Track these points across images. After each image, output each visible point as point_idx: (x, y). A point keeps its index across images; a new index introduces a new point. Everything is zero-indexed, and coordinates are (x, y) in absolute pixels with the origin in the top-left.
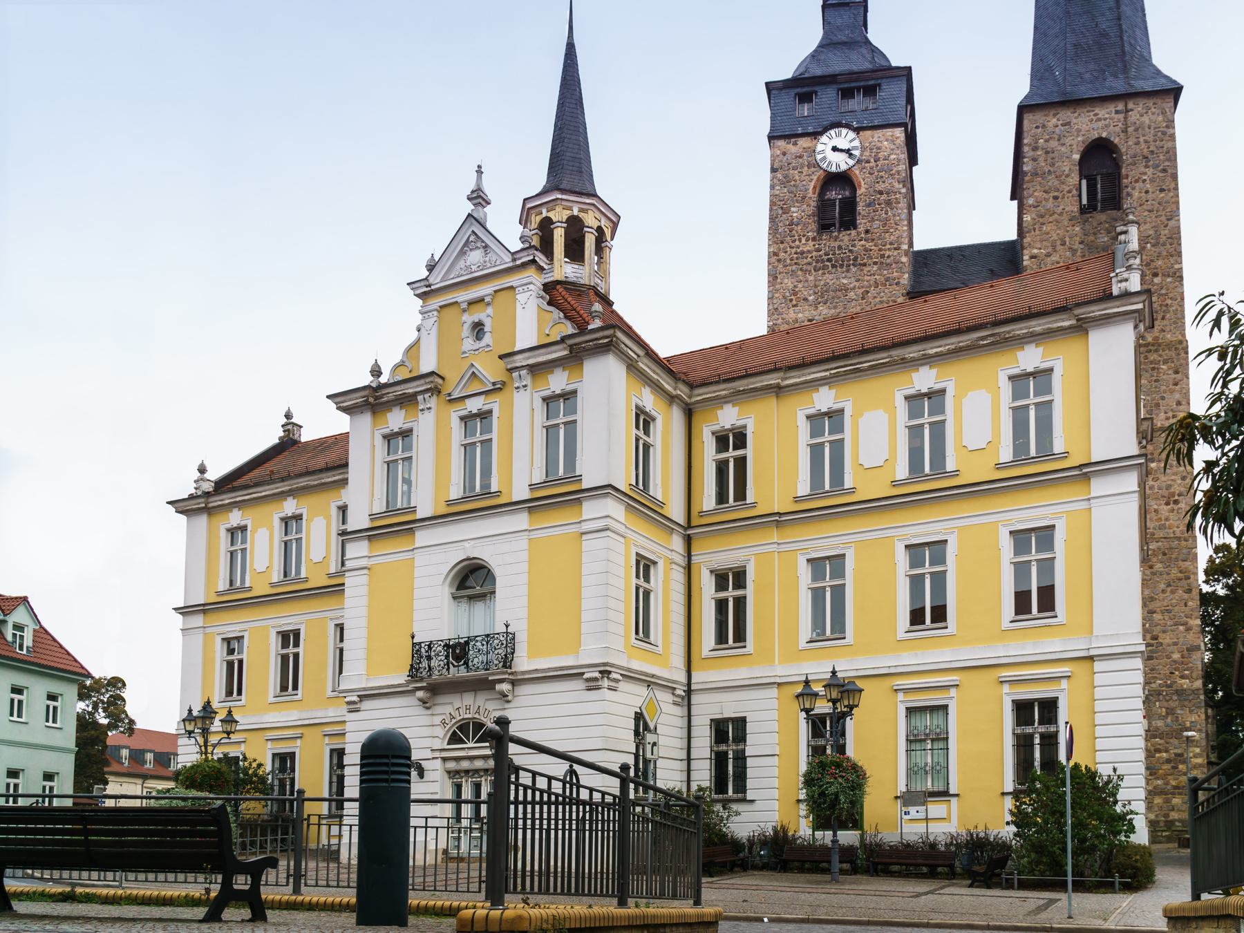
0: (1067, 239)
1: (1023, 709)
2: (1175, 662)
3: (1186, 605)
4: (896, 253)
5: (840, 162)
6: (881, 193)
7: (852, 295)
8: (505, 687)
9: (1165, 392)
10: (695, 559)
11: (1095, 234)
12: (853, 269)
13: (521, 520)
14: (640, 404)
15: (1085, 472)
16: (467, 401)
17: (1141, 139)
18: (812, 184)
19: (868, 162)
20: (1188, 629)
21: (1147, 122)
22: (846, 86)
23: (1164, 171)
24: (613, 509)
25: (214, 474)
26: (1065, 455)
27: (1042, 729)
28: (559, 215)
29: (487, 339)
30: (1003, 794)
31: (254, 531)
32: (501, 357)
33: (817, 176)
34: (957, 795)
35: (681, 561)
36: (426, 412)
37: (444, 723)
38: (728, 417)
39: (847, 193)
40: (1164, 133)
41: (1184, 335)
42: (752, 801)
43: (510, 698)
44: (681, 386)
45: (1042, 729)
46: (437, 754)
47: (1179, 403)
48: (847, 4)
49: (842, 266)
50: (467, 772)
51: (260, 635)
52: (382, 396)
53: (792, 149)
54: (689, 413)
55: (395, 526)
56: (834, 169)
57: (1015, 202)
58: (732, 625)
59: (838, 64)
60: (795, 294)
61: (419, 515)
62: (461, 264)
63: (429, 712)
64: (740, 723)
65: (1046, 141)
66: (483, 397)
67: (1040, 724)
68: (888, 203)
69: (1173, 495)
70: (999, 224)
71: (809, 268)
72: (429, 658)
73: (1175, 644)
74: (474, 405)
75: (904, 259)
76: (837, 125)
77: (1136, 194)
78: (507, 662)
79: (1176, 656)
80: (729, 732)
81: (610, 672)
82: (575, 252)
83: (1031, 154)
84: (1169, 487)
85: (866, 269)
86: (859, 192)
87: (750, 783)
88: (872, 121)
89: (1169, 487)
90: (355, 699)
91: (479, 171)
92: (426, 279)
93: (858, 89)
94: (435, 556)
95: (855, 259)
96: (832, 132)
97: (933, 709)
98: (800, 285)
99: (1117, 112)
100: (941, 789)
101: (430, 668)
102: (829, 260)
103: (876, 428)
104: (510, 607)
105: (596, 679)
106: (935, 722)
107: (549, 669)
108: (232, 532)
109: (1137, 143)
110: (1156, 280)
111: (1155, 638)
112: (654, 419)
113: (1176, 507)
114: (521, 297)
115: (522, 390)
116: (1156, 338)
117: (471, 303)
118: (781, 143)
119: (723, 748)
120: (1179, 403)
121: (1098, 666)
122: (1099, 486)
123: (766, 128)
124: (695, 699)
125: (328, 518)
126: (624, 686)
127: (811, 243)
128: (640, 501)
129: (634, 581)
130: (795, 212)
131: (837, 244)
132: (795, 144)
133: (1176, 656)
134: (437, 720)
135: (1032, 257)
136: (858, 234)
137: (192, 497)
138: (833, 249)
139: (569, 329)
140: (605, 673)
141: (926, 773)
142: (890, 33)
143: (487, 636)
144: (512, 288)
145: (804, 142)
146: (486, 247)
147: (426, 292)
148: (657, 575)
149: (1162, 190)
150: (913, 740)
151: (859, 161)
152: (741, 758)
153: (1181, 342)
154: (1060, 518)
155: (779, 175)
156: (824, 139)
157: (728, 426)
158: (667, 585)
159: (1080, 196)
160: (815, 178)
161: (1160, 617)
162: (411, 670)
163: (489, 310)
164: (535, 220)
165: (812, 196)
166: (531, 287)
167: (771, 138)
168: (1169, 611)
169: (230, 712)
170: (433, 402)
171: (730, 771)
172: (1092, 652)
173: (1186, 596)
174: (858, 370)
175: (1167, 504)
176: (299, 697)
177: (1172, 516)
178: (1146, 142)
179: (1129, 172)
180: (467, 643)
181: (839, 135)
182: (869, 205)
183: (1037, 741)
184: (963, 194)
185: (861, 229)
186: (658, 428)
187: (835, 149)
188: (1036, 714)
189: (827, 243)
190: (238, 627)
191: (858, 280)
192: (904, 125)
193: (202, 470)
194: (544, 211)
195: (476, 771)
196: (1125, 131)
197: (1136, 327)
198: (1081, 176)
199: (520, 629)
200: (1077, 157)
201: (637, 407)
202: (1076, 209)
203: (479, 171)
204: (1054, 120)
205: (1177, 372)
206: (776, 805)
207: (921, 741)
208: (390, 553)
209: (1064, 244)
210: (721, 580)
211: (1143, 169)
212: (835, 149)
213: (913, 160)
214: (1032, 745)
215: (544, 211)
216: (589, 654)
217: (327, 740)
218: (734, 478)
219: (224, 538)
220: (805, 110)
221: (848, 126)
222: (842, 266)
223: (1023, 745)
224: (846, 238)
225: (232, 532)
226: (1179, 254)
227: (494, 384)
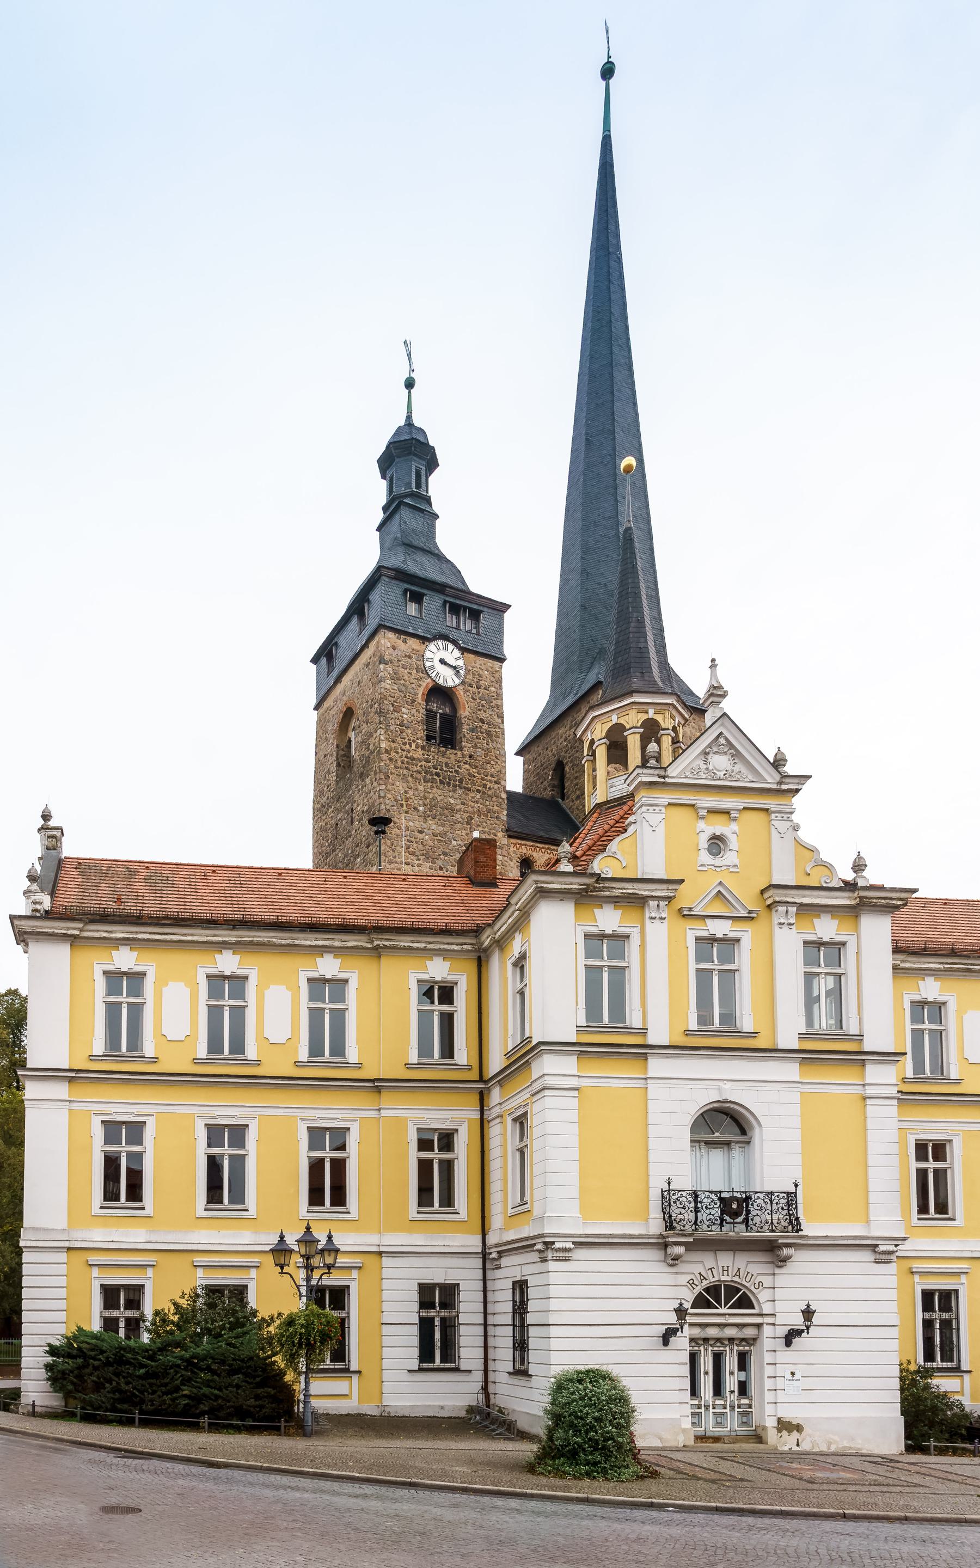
4: (496, 786)
5: (448, 678)
6: (482, 721)
12: (460, 791)
16: (708, 921)
22: (475, 607)
29: (729, 858)
31: (160, 984)
33: (426, 684)
36: (657, 922)
37: (691, 1283)
39: (448, 710)
49: (449, 784)
50: (731, 1340)
52: (601, 890)
56: (441, 682)
66: (730, 922)
68: (489, 734)
71: (419, 776)
74: (720, 928)
76: (445, 637)
81: (877, 1246)
88: (476, 646)
91: (713, 665)
94: (680, 1091)
95: (461, 781)
96: (440, 642)
98: (411, 792)
105: (569, 1250)
107: (842, 1238)
108: (113, 978)
115: (785, 928)
117: (711, 811)
125: (296, 990)
127: (420, 751)
131: (444, 760)
132: (405, 642)
134: (684, 1279)
136: (464, 756)
138: (440, 764)
145: (413, 643)
151: (463, 683)
156: (432, 646)
160: (424, 684)
163: (734, 826)
169: (308, 1228)
174: (969, 970)
176: (149, 1211)
180: (748, 1198)
181: (446, 649)
191: (463, 804)
194: (651, 712)
212: (442, 661)
215: (651, 712)
220: (412, 609)
221: (454, 642)
224: (453, 757)
225: (113, 978)
227: (750, 912)
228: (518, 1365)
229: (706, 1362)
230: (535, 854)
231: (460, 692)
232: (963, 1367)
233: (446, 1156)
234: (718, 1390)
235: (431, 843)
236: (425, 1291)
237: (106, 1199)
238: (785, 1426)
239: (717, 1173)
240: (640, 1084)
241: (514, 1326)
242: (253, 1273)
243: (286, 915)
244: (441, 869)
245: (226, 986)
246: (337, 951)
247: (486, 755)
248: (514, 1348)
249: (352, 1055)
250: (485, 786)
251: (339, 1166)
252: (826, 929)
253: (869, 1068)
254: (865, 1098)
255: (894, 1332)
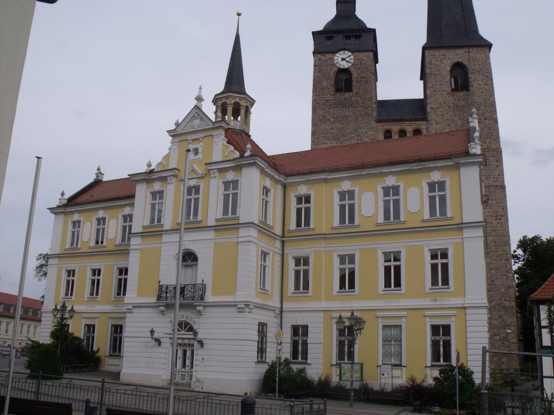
0: (446, 102)
1: (435, 329)
2: (502, 293)
3: (506, 266)
5: (345, 65)
6: (363, 78)
7: (350, 119)
8: (200, 308)
9: (493, 170)
10: (286, 251)
11: (458, 100)
12: (351, 109)
13: (211, 235)
14: (265, 185)
15: (460, 227)
17: (476, 63)
18: (332, 73)
19: (357, 65)
20: (508, 278)
21: (478, 57)
23: (487, 77)
24: (253, 233)
25: (68, 195)
26: (451, 218)
27: (444, 338)
28: (231, 101)
29: (200, 156)
30: (426, 367)
31: (109, 220)
32: (206, 164)
34: (405, 366)
35: (280, 252)
36: (170, 184)
38: (303, 190)
40: (486, 62)
41: (500, 146)
42: (310, 364)
43: (202, 313)
44: (282, 176)
45: (444, 338)
46: (167, 336)
47: (499, 175)
48: (347, 2)
51: (84, 269)
53: (323, 58)
54: (285, 186)
55: (154, 231)
56: (342, 67)
57: (422, 81)
58: (303, 283)
59: (343, 26)
60: (324, 117)
61: (165, 228)
62: (190, 124)
63: (165, 316)
64: (305, 328)
65: (436, 61)
67: (443, 335)
68: (367, 82)
69: (498, 216)
70: (414, 90)
72: (166, 293)
73: (502, 285)
74: (192, 183)
75: (374, 105)
77: (475, 85)
78: (202, 298)
79: (503, 290)
80: (300, 332)
81: (249, 305)
82: (236, 113)
83: (429, 66)
84: (496, 212)
85: (357, 109)
86: (353, 77)
87: (309, 356)
89: (496, 212)
90: (131, 307)
91: (200, 88)
92: (174, 130)
93: (353, 36)
94: (169, 250)
95: (352, 104)
96: (341, 52)
97: (395, 326)
98: (327, 114)
99: (465, 52)
100: (398, 363)
101: (167, 297)
102: (340, 104)
103: (369, 203)
104: (204, 272)
105: (243, 308)
106: (396, 333)
108: (74, 223)
109: (475, 65)
110: (486, 122)
111: (492, 281)
112: (270, 190)
113: (500, 221)
114: (216, 140)
116: (487, 146)
117: (193, 140)
118: (319, 55)
119: (297, 338)
120: (499, 175)
121: (468, 311)
122: (467, 233)
123: (312, 48)
124: (284, 315)
125: (117, 220)
126: (255, 311)
127: (332, 97)
128: (264, 229)
129: (260, 263)
130: (325, 84)
131: (343, 97)
132: (325, 56)
133: (503, 290)
135: (431, 108)
137: (59, 207)
139: (237, 154)
140: (247, 306)
141: (391, 355)
142: (365, 11)
143: (194, 285)
144: (212, 135)
145: (329, 56)
146: (202, 118)
147: (173, 134)
148: (269, 259)
149: (486, 85)
150: (386, 340)
152: (305, 344)
153: (498, 149)
154: (450, 245)
155: (317, 68)
156: (338, 55)
157: (302, 194)
158: (273, 262)
159: (451, 84)
161: (495, 272)
162: (158, 297)
163: (201, 144)
164: (220, 103)
165: (332, 77)
166: (221, 136)
167: (314, 53)
168: (499, 269)
169: (64, 303)
170: (174, 180)
171: (299, 349)
172: (465, 305)
173: (506, 262)
175: (496, 220)
176: (73, 300)
177: (498, 225)
178: (478, 64)
179: (472, 76)
181: (344, 54)
182: (358, 82)
183: (441, 343)
184: (399, 77)
185: (355, 92)
186: (271, 194)
187: (343, 59)
188: (441, 331)
189: (340, 96)
190: (73, 266)
192: (373, 51)
193: (63, 194)
195: (185, 344)
196: (469, 60)
197: (479, 167)
198: (451, 76)
199: (209, 283)
200: (449, 69)
201: (264, 186)
202: (449, 89)
203: (200, 88)
204: (438, 54)
205: (497, 161)
206: (321, 367)
207: (389, 340)
208: (151, 244)
209: (445, 103)
210: (298, 261)
211: (477, 75)
213: (376, 61)
214: (439, 345)
216: (240, 296)
217: (110, 320)
218: (304, 218)
219: (70, 225)
221: (348, 50)
222: (346, 107)
223: (435, 345)
224: (348, 95)
225: (74, 223)
226: (496, 112)
228: (259, 359)
229: (180, 354)
230: (392, 128)
231: (352, 70)
232: (403, 365)
233: (444, 261)
234: (184, 366)
235: (336, 133)
236: (435, 329)
237: (385, 287)
238: (198, 380)
239: (187, 277)
240: (159, 245)
241: (258, 342)
242: (97, 320)
243: (115, 195)
244: (341, 143)
245: (101, 221)
246: (103, 208)
247: (365, 91)
248: (258, 352)
249: (449, 214)
250: (364, 104)
251: (398, 269)
252: (230, 176)
253: (241, 230)
254: (238, 243)
255: (322, 346)
